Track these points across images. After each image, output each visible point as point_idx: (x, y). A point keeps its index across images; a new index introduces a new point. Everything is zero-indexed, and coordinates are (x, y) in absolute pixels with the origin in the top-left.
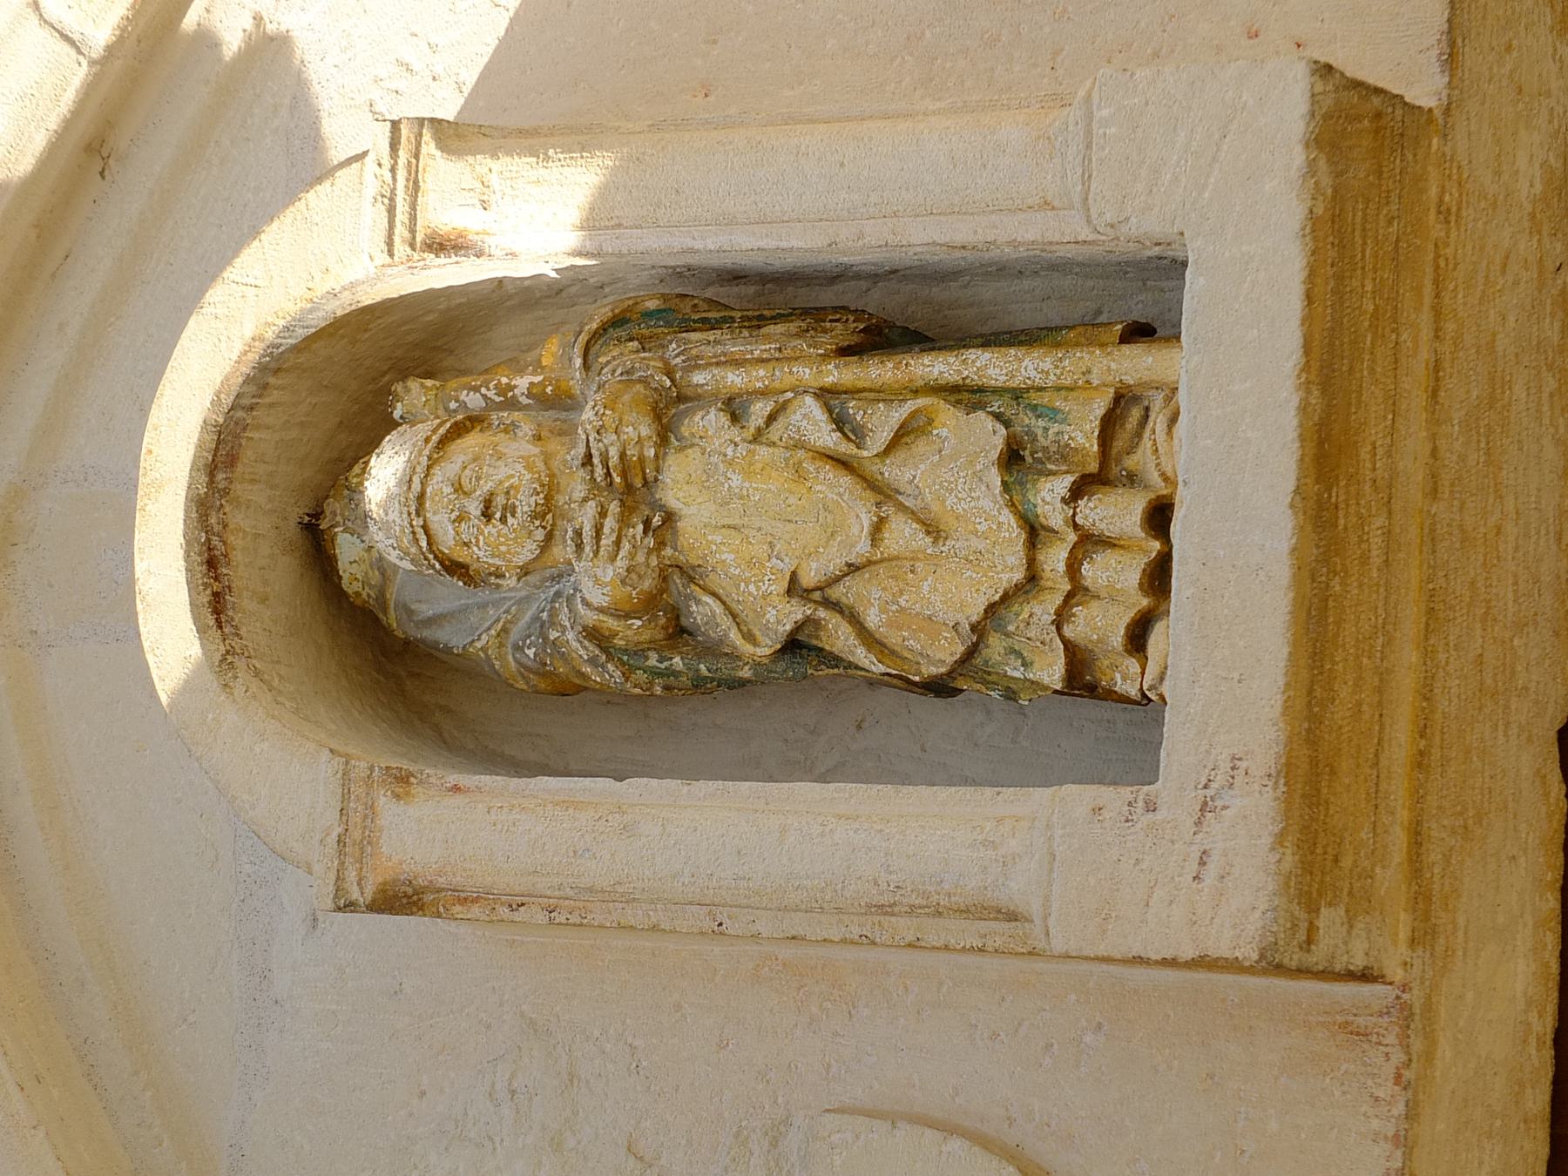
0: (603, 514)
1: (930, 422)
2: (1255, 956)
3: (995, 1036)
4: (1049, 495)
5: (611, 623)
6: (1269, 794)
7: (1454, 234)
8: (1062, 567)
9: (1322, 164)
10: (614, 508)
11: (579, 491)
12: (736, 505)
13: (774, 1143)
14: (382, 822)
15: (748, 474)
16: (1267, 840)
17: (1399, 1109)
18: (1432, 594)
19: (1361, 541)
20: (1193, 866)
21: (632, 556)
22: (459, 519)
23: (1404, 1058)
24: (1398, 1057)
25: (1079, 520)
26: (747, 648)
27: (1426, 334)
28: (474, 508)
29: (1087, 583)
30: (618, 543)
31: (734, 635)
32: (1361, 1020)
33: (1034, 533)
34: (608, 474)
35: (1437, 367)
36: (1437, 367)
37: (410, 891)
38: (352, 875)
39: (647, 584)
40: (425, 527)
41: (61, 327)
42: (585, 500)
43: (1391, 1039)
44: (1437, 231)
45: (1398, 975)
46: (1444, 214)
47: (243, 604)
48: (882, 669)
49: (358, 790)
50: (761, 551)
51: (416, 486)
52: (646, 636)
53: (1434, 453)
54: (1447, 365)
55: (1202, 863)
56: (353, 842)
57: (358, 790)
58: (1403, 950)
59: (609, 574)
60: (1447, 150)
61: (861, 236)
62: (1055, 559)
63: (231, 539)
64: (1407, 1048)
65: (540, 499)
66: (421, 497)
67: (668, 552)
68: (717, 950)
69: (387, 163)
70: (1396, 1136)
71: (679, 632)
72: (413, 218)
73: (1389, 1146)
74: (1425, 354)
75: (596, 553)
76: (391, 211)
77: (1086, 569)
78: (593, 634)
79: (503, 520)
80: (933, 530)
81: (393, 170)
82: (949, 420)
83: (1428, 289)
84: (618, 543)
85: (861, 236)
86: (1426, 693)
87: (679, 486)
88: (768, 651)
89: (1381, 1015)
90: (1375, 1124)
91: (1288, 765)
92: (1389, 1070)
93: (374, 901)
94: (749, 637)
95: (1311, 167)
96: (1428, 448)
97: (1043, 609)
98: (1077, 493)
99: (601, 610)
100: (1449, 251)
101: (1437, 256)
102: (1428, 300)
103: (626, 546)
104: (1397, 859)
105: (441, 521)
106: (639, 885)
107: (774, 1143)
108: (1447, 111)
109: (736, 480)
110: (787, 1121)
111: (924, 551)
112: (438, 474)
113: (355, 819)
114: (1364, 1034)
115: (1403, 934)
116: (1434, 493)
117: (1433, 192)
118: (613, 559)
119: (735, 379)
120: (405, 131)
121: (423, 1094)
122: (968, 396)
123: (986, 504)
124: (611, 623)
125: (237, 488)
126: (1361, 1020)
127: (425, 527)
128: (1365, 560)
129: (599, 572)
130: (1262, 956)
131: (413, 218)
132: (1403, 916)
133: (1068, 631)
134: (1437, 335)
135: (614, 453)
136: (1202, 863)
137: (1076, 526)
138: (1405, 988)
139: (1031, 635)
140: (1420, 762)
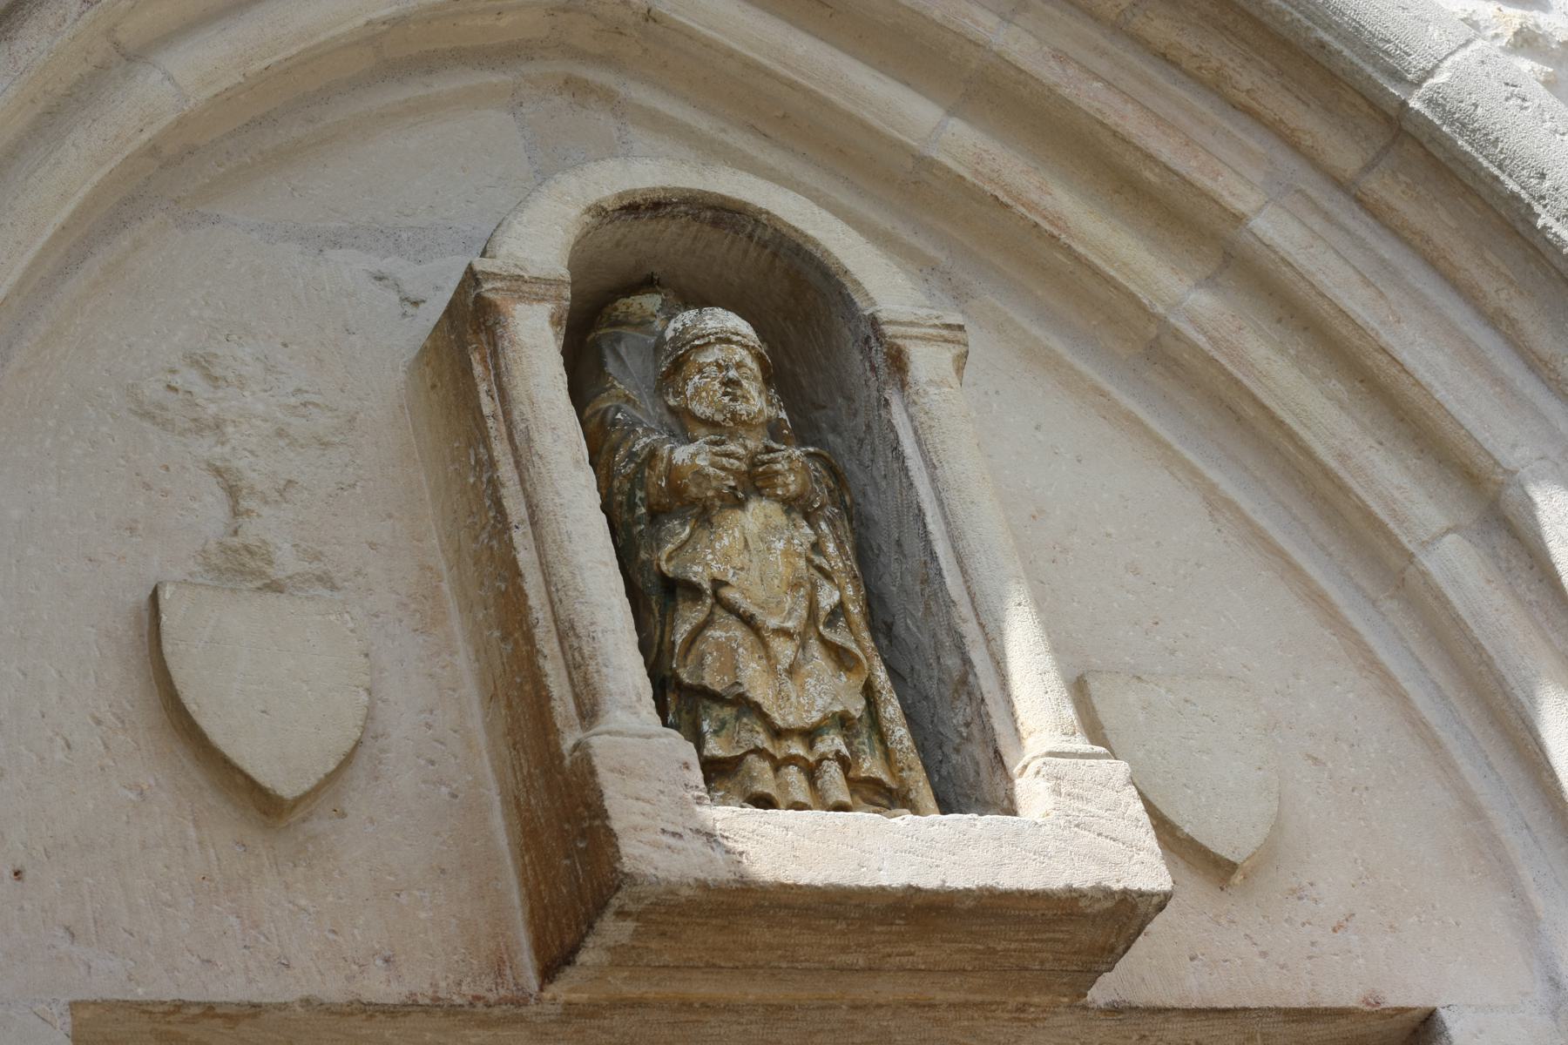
0: (738, 459)
1: (849, 670)
2: (626, 870)
3: (429, 726)
4: (833, 742)
5: (662, 467)
6: (731, 876)
7: (1007, 1016)
8: (793, 751)
9: (1109, 904)
10: (744, 467)
11: (751, 444)
12: (762, 546)
13: (319, 579)
14: (536, 306)
15: (785, 553)
16: (702, 876)
17: (458, 1000)
18: (791, 1008)
19: (858, 945)
20: (671, 828)
21: (716, 477)
22: (718, 365)
23: (492, 1001)
24: (492, 997)
25: (825, 763)
26: (664, 557)
27: (954, 997)
28: (732, 374)
29: (784, 770)
30: (723, 468)
31: (670, 547)
32: (508, 972)
33: (810, 735)
34: (763, 463)
35: (932, 1006)
36: (932, 1006)
37: (489, 324)
38: (499, 284)
39: (693, 490)
40: (709, 344)
41: (723, 130)
42: (745, 447)
43: (502, 992)
44: (1012, 1003)
45: (547, 995)
46: (1021, 1009)
47: (644, 228)
48: (679, 641)
49: (553, 291)
50: (737, 562)
51: (735, 338)
52: (652, 490)
53: (879, 1006)
54: (931, 1014)
55: (674, 834)
56: (523, 286)
57: (553, 291)
58: (563, 998)
59: (702, 462)
60: (1061, 1009)
61: (965, 621)
62: (797, 748)
63: (664, 222)
64: (499, 1003)
65: (744, 418)
66: (729, 341)
67: (718, 503)
68: (435, 541)
69: (937, 322)
70: (439, 999)
71: (657, 515)
72: (911, 338)
73: (430, 993)
74: (940, 997)
75: (716, 454)
76: (912, 324)
77: (793, 769)
78: (653, 454)
79: (725, 394)
80: (792, 671)
81: (935, 326)
82: (853, 682)
83: (978, 998)
84: (723, 468)
85: (965, 621)
86: (731, 1008)
87: (758, 515)
88: (664, 567)
89: (516, 985)
90: (443, 984)
91: (749, 890)
92: (481, 992)
93: (483, 298)
94: (669, 559)
95: (1108, 893)
96: (882, 1001)
97: (762, 740)
98: (839, 757)
99: (670, 460)
100: (999, 1013)
101: (998, 1003)
102: (971, 997)
103: (723, 474)
104: (625, 989)
105: (709, 357)
106: (543, 470)
107: (319, 579)
108: (1085, 1008)
109: (780, 545)
110: (333, 588)
111: (778, 662)
112: (745, 353)
113: (535, 289)
114: (500, 974)
115: (574, 997)
116: (855, 1007)
117: (1036, 1000)
118: (713, 465)
119: (831, 548)
120: (960, 335)
121: (285, 345)
122: (869, 690)
123: (820, 703)
124: (662, 467)
125: (695, 227)
126: (508, 972)
127: (709, 344)
128: (844, 949)
129: (702, 456)
130: (627, 875)
131: (911, 338)
132: (585, 996)
133: (751, 758)
134: (952, 1005)
135: (778, 467)
136: (674, 834)
137: (820, 762)
138: (539, 1000)
139: (742, 734)
140: (686, 1005)
